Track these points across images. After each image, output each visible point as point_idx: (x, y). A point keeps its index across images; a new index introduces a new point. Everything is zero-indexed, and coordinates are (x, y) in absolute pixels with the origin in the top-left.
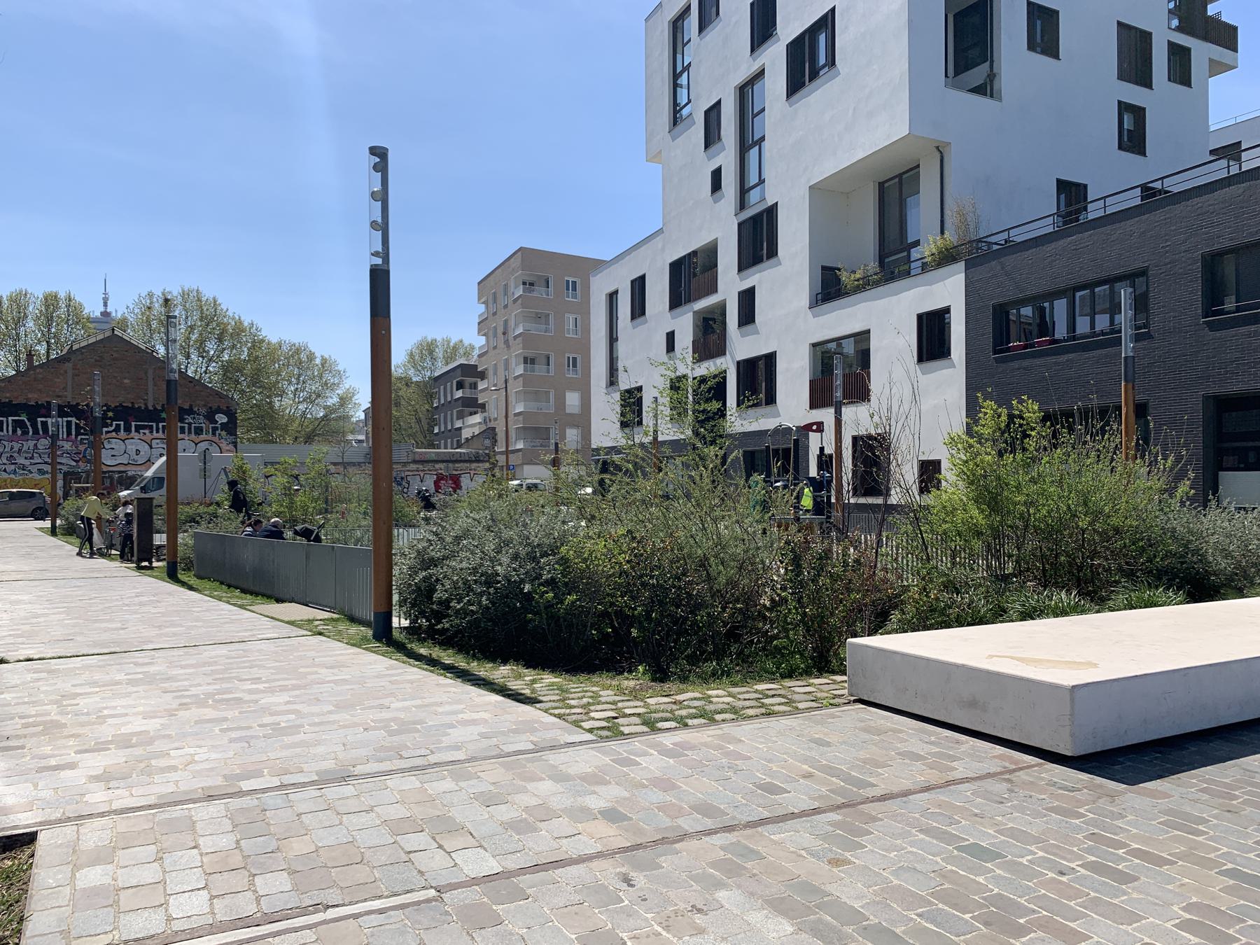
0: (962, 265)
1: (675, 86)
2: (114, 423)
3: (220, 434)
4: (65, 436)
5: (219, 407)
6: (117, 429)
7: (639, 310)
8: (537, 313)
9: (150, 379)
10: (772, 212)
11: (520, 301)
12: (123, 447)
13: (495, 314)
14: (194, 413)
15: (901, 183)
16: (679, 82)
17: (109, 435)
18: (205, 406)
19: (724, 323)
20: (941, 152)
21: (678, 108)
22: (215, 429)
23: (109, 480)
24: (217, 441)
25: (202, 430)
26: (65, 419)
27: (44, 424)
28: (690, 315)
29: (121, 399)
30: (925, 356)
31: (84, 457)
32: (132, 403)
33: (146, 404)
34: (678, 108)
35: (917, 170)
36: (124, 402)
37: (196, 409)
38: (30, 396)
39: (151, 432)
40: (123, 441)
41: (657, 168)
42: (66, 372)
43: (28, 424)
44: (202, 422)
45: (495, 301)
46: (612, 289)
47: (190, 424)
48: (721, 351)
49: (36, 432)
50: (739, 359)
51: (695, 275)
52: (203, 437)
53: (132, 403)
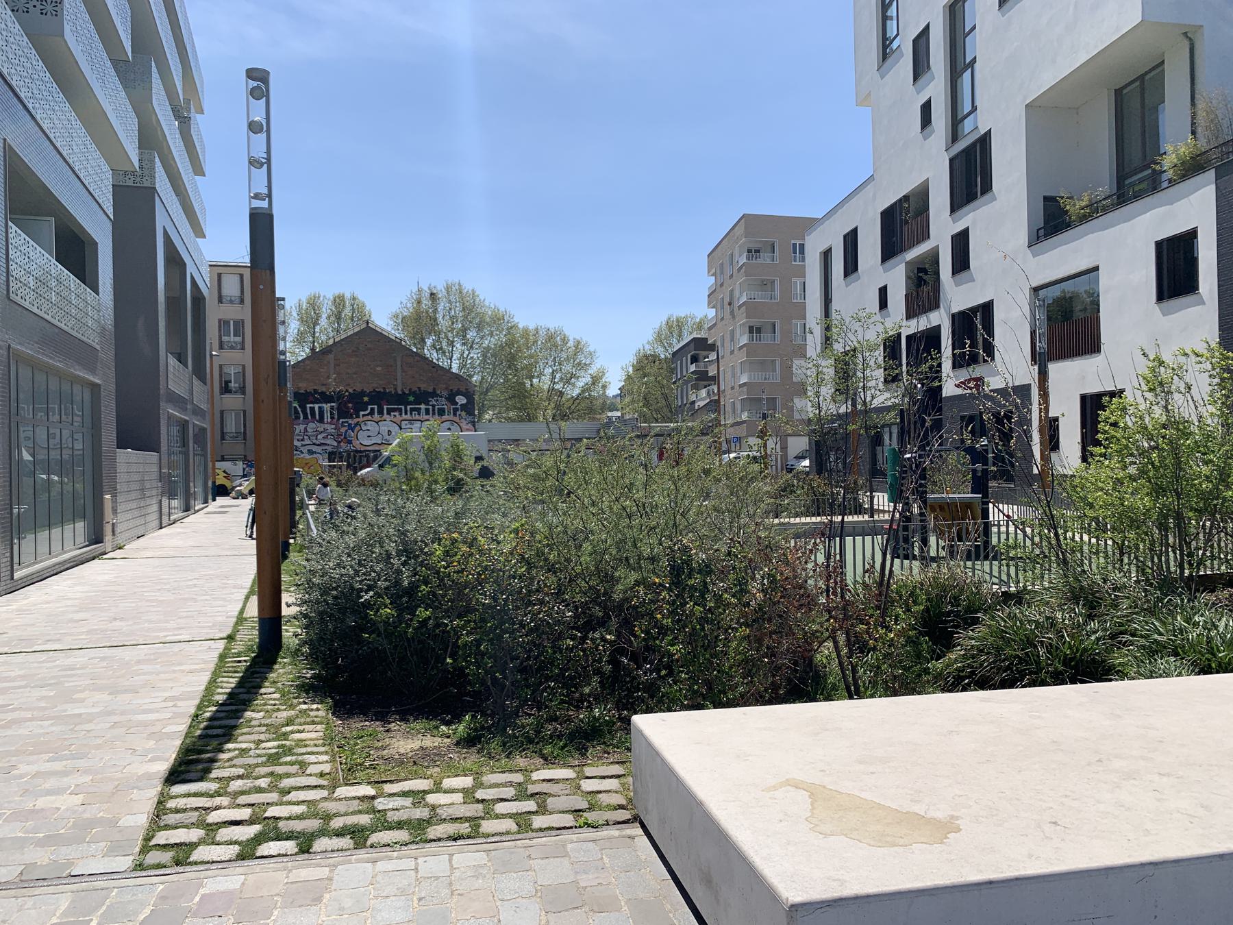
0: (1211, 174)
1: (885, 19)
2: (369, 407)
3: (460, 415)
4: (329, 420)
5: (458, 389)
6: (372, 413)
7: (851, 266)
8: (763, 281)
9: (399, 367)
10: (985, 141)
11: (743, 270)
12: (377, 429)
13: (722, 285)
14: (437, 395)
15: (1143, 82)
16: (889, 14)
17: (365, 418)
18: (446, 388)
19: (937, 273)
20: (1190, 39)
21: (888, 42)
22: (455, 410)
23: (365, 459)
24: (457, 420)
25: (444, 412)
26: (329, 405)
27: (312, 409)
28: (902, 267)
29: (375, 385)
30: (1166, 294)
31: (345, 438)
32: (384, 388)
33: (395, 389)
34: (888, 42)
35: (1161, 68)
36: (377, 388)
37: (439, 392)
38: (300, 385)
39: (401, 414)
40: (377, 423)
41: (866, 112)
42: (329, 362)
43: (299, 409)
44: (443, 403)
45: (722, 273)
46: (824, 247)
47: (433, 406)
48: (934, 304)
49: (306, 417)
50: (955, 310)
51: (906, 222)
52: (445, 417)
53: (384, 388)
